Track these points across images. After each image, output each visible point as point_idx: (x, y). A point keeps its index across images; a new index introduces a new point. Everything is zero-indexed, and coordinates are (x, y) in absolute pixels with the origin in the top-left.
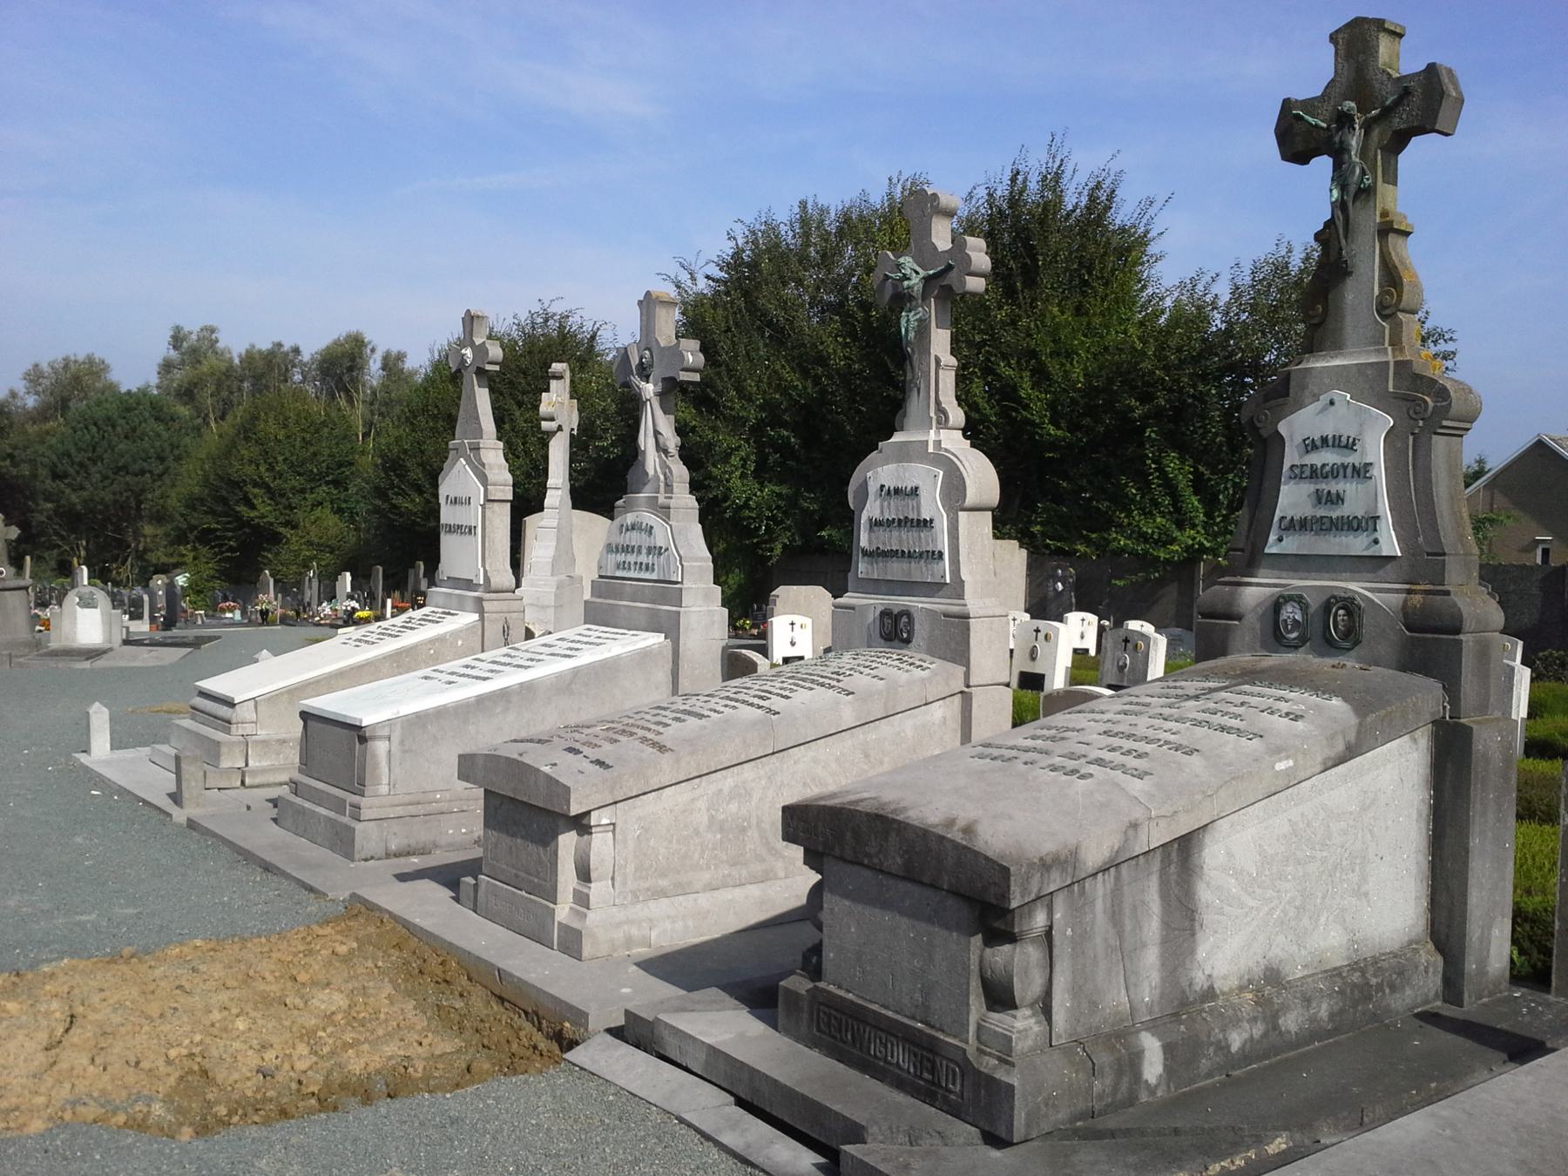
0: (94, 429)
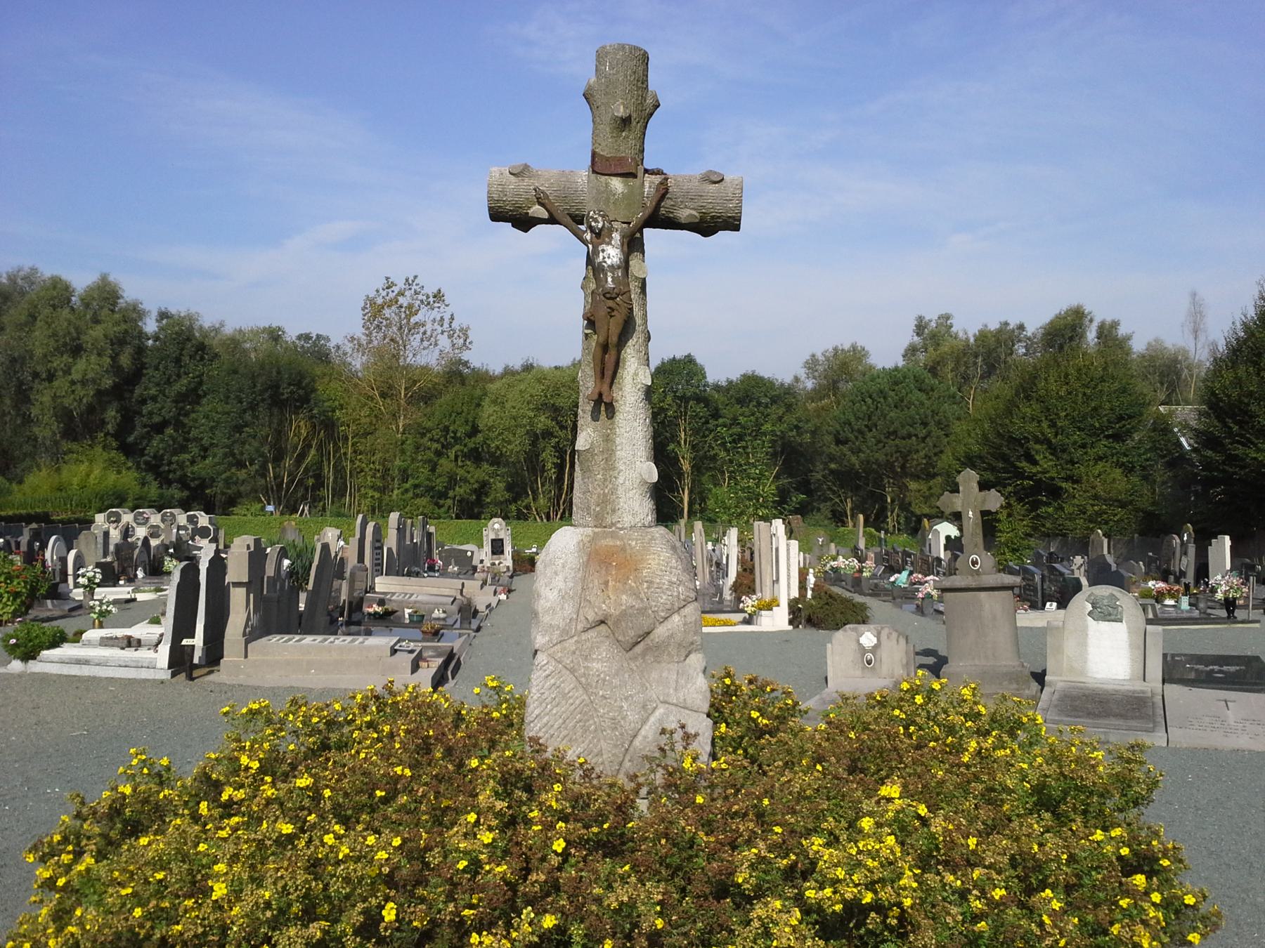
0: (869, 401)
